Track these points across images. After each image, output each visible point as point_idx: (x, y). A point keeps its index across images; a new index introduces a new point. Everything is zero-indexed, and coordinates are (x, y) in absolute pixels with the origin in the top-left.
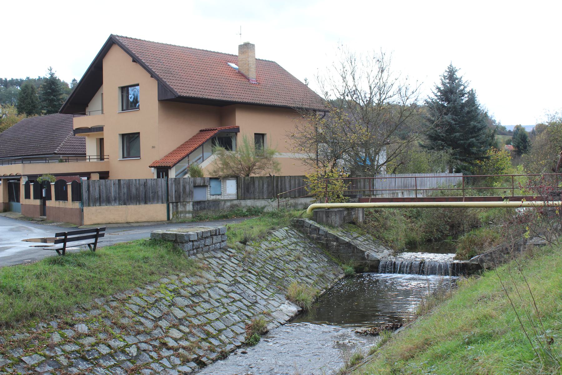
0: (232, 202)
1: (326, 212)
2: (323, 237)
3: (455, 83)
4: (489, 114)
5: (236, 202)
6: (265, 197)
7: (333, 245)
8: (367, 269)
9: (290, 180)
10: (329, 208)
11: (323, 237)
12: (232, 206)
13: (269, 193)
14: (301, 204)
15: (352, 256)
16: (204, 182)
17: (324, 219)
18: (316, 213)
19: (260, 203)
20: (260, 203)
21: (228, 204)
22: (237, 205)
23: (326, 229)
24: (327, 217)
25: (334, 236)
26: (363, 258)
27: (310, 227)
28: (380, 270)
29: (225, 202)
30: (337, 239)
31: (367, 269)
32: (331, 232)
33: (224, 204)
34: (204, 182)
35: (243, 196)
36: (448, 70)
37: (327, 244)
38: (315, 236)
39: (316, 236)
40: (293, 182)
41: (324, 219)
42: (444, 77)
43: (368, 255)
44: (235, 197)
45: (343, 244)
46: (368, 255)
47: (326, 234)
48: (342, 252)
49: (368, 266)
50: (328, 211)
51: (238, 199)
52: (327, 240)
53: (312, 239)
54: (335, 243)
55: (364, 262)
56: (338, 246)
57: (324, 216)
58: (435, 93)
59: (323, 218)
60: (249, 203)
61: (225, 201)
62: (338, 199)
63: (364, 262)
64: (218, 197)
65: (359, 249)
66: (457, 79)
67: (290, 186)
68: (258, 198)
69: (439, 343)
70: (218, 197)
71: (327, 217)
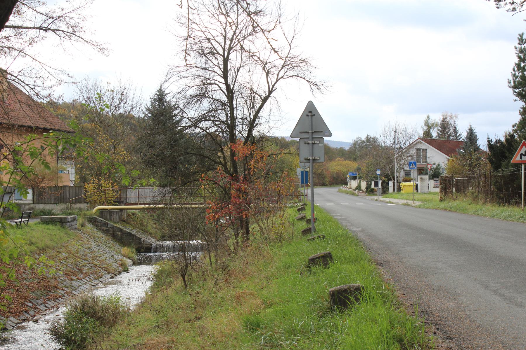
0: (30, 206)
1: (110, 212)
2: (111, 229)
3: (164, 105)
4: (103, 86)
5: (32, 206)
6: (52, 203)
7: (118, 235)
8: (143, 250)
9: (70, 190)
10: (110, 209)
11: (111, 229)
12: (30, 209)
13: (55, 199)
14: (77, 208)
15: (132, 242)
16: (11, 190)
17: (108, 217)
18: (102, 213)
19: (48, 207)
20: (48, 207)
21: (27, 207)
22: (32, 209)
23: (112, 224)
24: (111, 215)
25: (119, 228)
26: (140, 243)
27: (101, 223)
28: (152, 251)
29: (25, 206)
30: (121, 230)
31: (143, 250)
32: (115, 225)
33: (24, 207)
34: (11, 190)
35: (37, 201)
36: (158, 93)
37: (113, 234)
38: (105, 228)
39: (105, 228)
40: (71, 191)
41: (108, 217)
42: (154, 99)
43: (143, 241)
44: (31, 202)
45: (126, 233)
46: (143, 241)
47: (113, 227)
48: (125, 239)
49: (143, 248)
50: (110, 212)
51: (33, 203)
52: (113, 231)
53: (103, 230)
54: (119, 233)
55: (141, 245)
56: (121, 235)
57: (108, 215)
58: (144, 111)
59: (107, 217)
60: (41, 207)
61: (25, 204)
62: (109, 204)
63: (141, 245)
64: (20, 201)
65: (137, 237)
66: (166, 102)
67: (70, 194)
68: (47, 203)
69: (173, 327)
70: (20, 201)
71: (111, 215)
